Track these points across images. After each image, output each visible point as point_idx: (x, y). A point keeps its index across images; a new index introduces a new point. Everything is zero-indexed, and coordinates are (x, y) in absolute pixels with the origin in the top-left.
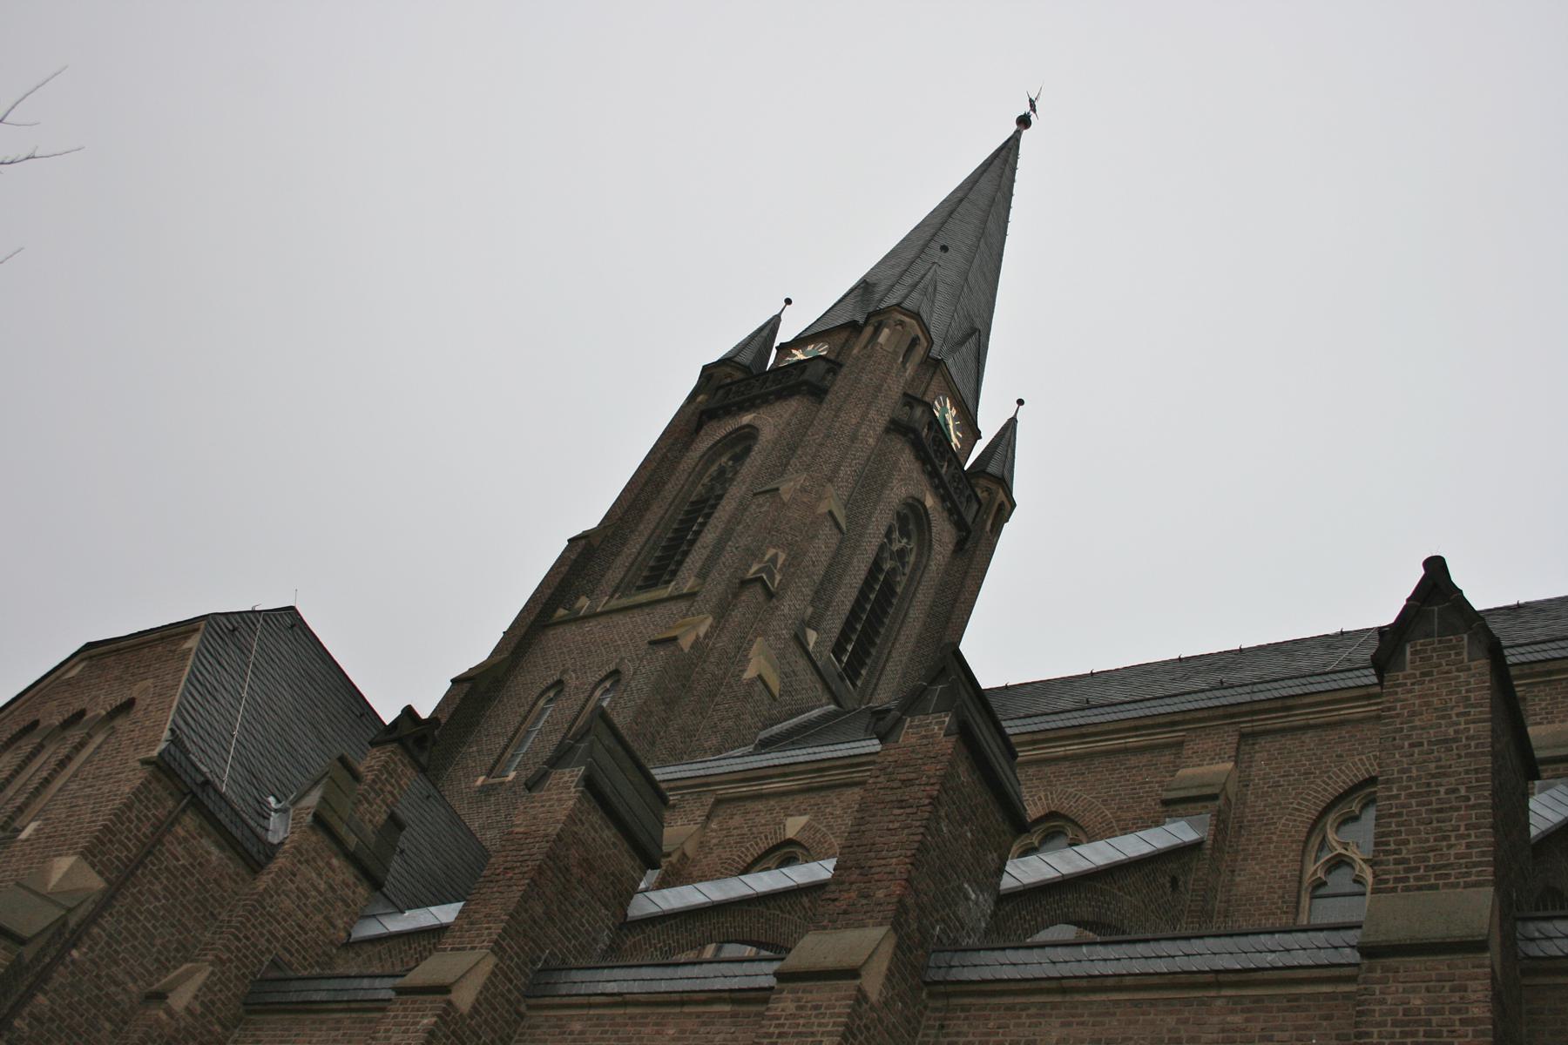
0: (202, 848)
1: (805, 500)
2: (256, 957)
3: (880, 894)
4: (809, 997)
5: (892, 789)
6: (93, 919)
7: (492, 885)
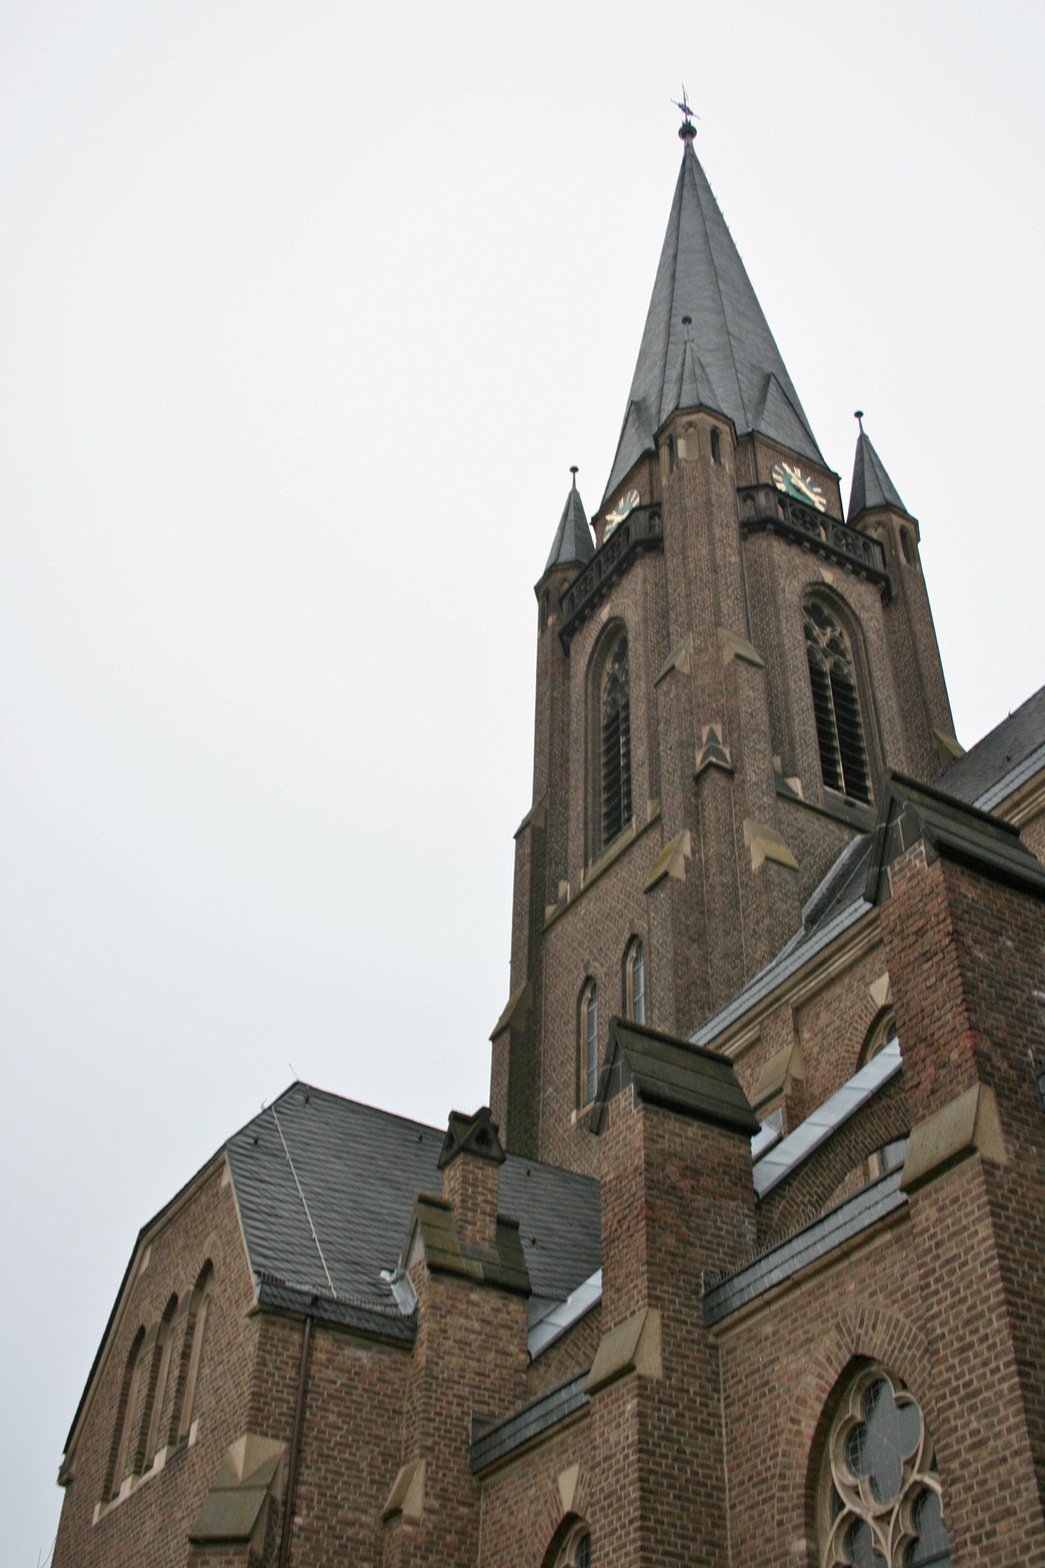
0: (349, 1358)
1: (706, 659)
2: (457, 1426)
3: (954, 1056)
4: (942, 1194)
5: (910, 946)
6: (294, 1480)
7: (616, 1243)
